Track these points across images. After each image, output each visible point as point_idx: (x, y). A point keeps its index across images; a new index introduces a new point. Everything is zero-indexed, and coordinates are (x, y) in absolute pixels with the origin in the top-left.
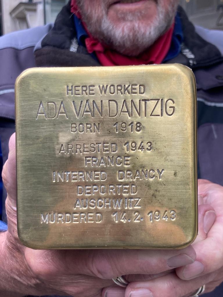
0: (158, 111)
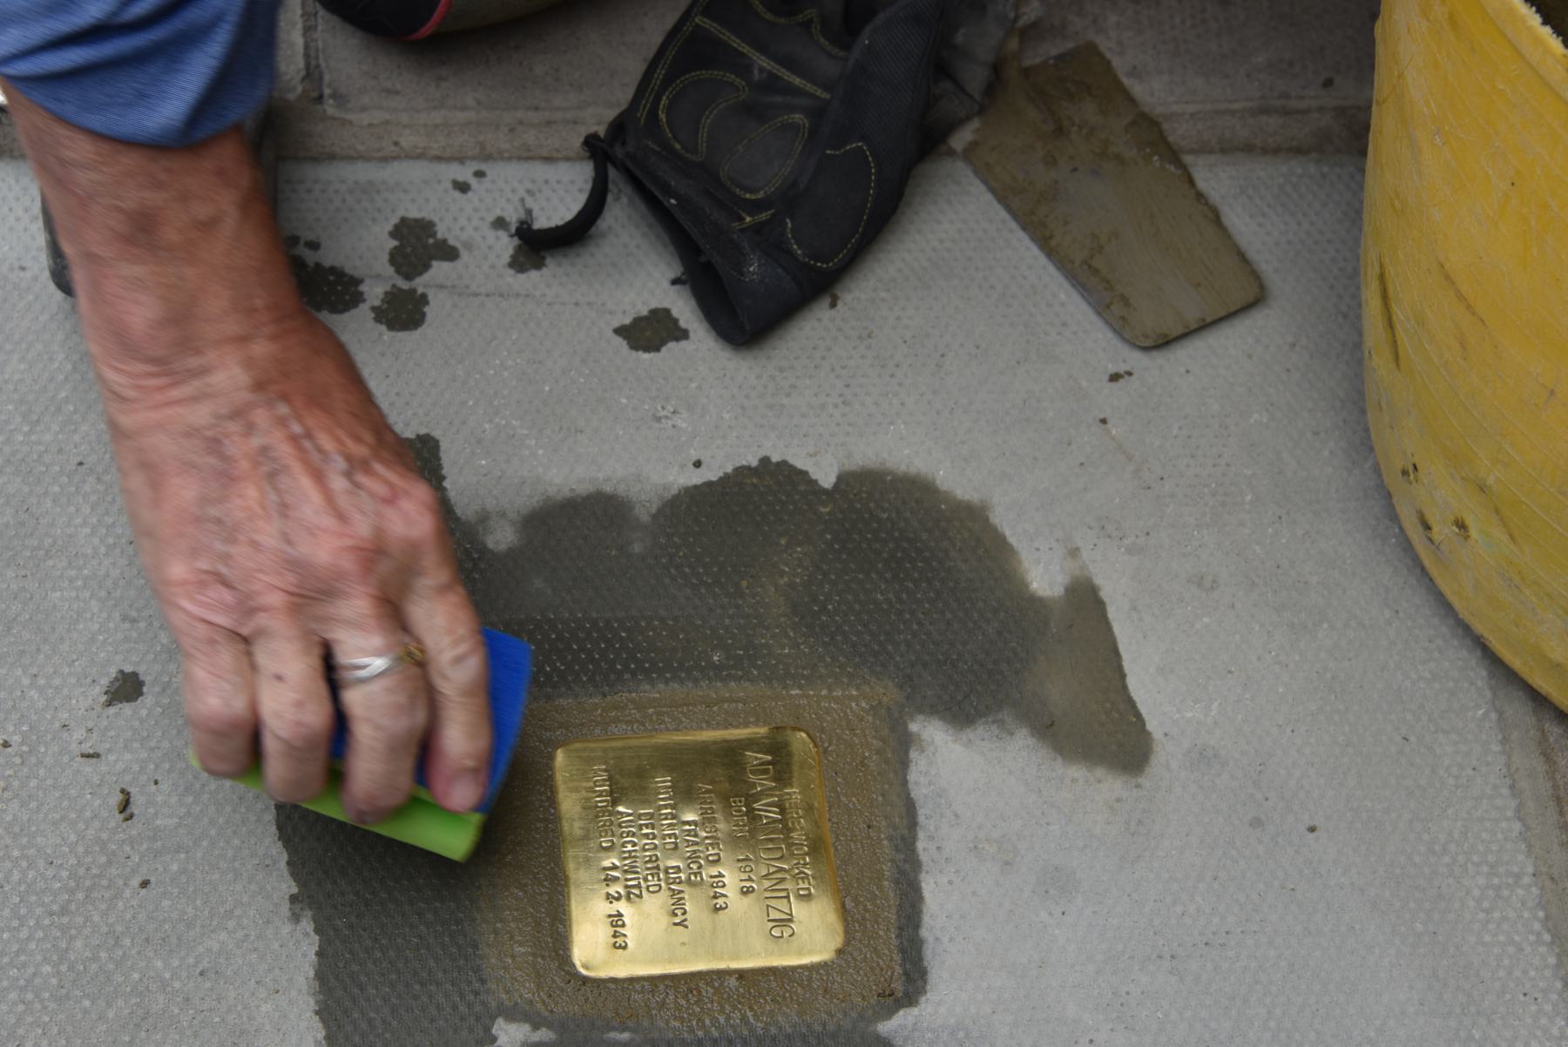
0: (774, 915)
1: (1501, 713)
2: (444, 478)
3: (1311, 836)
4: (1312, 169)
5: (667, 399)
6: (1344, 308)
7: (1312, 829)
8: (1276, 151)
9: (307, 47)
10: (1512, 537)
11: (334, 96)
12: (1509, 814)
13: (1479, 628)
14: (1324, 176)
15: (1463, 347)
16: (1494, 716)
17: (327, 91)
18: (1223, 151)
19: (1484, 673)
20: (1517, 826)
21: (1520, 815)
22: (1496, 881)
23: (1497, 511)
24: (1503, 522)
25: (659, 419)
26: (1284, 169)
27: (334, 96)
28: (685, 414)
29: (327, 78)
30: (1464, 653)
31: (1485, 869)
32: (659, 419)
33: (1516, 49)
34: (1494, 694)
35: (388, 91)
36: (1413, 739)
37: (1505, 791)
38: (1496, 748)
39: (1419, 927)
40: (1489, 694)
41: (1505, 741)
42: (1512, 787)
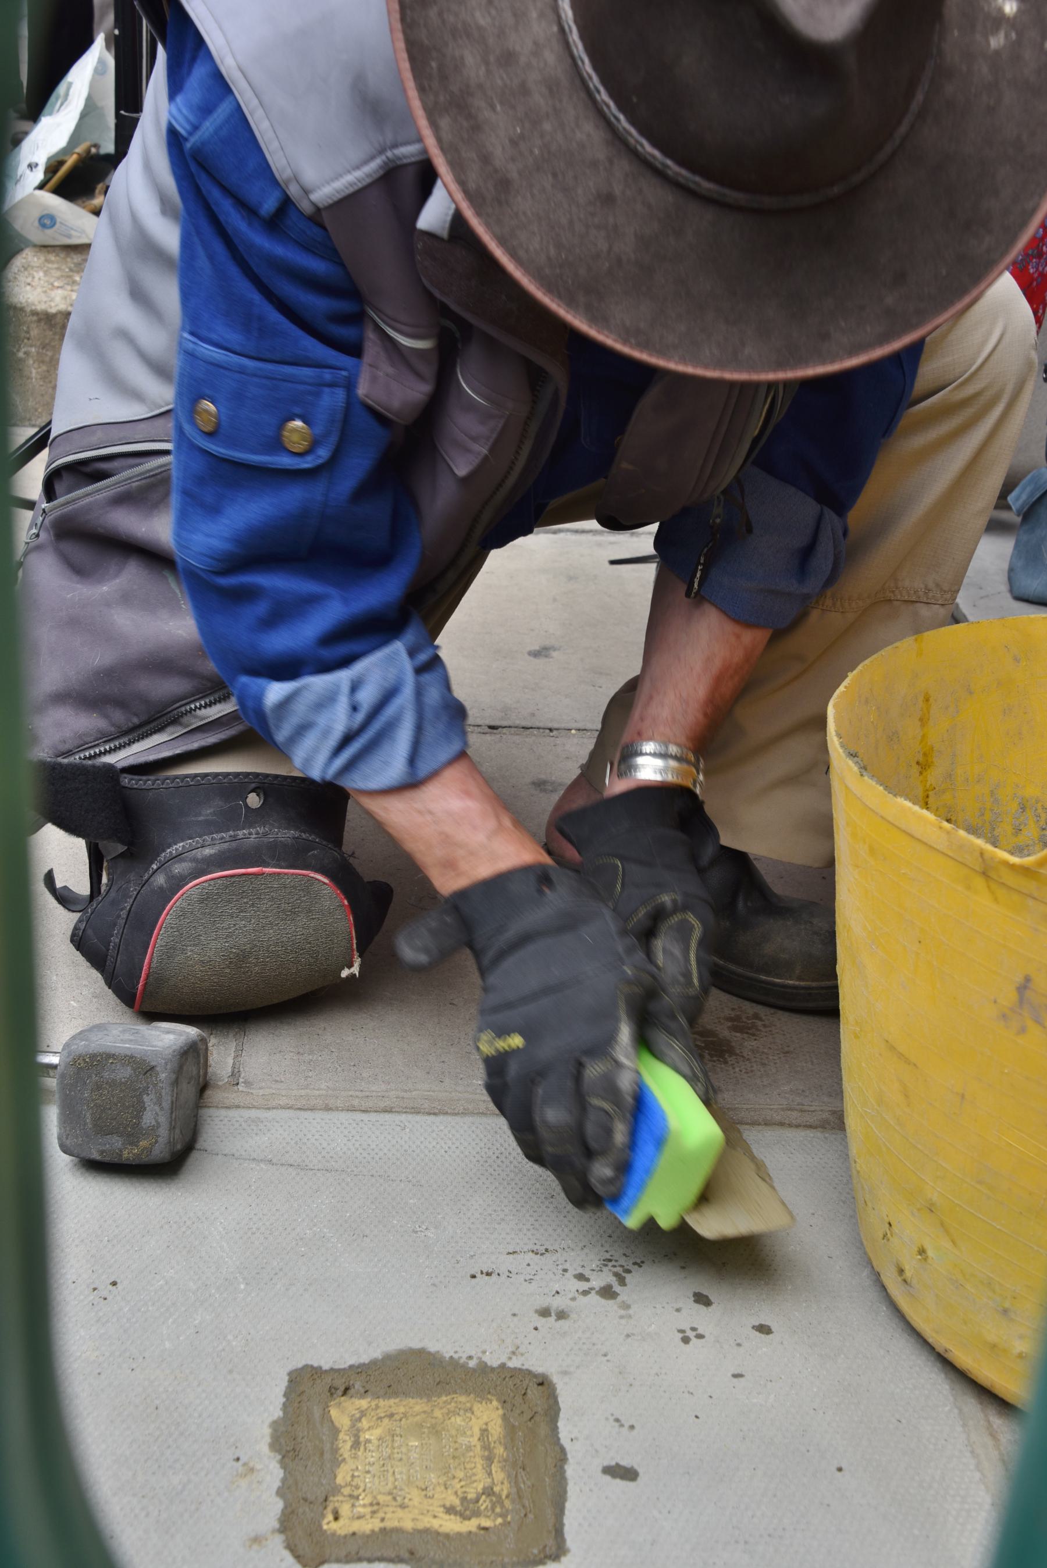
1: (960, 1410)
2: (321, 1368)
3: (839, 1474)
4: (819, 1134)
5: (423, 1222)
6: (843, 1198)
7: (840, 1469)
8: (798, 1126)
9: (234, 1064)
10: (954, 1242)
11: (245, 1083)
12: (972, 1467)
13: (941, 1342)
14: (826, 1138)
15: (907, 1096)
16: (956, 1411)
17: (241, 1080)
18: (766, 1124)
19: (947, 1387)
20: (977, 1475)
21: (978, 1467)
22: (967, 1506)
23: (942, 1224)
24: (947, 1232)
25: (416, 1232)
26: (803, 1134)
27: (245, 1083)
28: (433, 1230)
29: (242, 1075)
30: (933, 1375)
31: (958, 1499)
32: (416, 1232)
33: (925, 844)
34: (955, 1399)
35: (277, 1081)
36: (903, 1421)
37: (968, 1454)
38: (959, 1429)
39: (916, 1532)
40: (951, 1399)
41: (964, 1425)
42: (972, 1452)
